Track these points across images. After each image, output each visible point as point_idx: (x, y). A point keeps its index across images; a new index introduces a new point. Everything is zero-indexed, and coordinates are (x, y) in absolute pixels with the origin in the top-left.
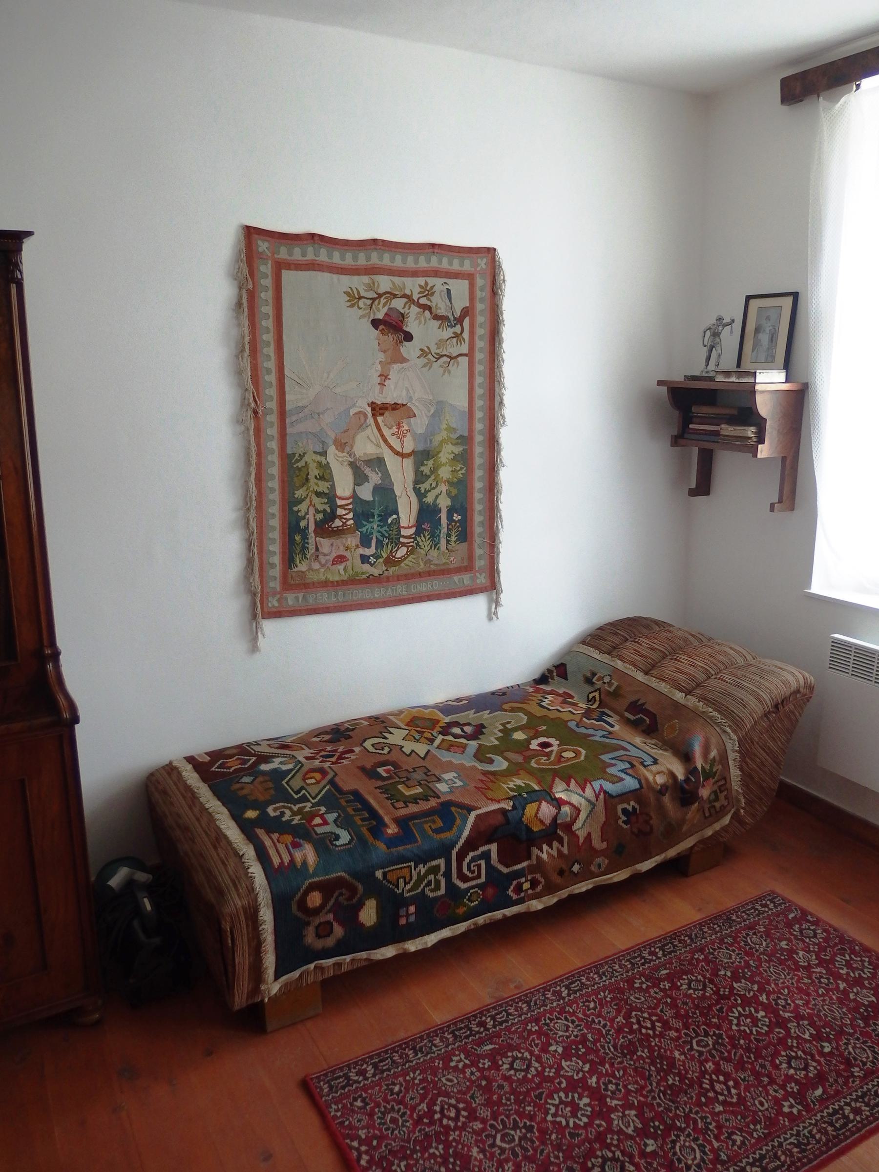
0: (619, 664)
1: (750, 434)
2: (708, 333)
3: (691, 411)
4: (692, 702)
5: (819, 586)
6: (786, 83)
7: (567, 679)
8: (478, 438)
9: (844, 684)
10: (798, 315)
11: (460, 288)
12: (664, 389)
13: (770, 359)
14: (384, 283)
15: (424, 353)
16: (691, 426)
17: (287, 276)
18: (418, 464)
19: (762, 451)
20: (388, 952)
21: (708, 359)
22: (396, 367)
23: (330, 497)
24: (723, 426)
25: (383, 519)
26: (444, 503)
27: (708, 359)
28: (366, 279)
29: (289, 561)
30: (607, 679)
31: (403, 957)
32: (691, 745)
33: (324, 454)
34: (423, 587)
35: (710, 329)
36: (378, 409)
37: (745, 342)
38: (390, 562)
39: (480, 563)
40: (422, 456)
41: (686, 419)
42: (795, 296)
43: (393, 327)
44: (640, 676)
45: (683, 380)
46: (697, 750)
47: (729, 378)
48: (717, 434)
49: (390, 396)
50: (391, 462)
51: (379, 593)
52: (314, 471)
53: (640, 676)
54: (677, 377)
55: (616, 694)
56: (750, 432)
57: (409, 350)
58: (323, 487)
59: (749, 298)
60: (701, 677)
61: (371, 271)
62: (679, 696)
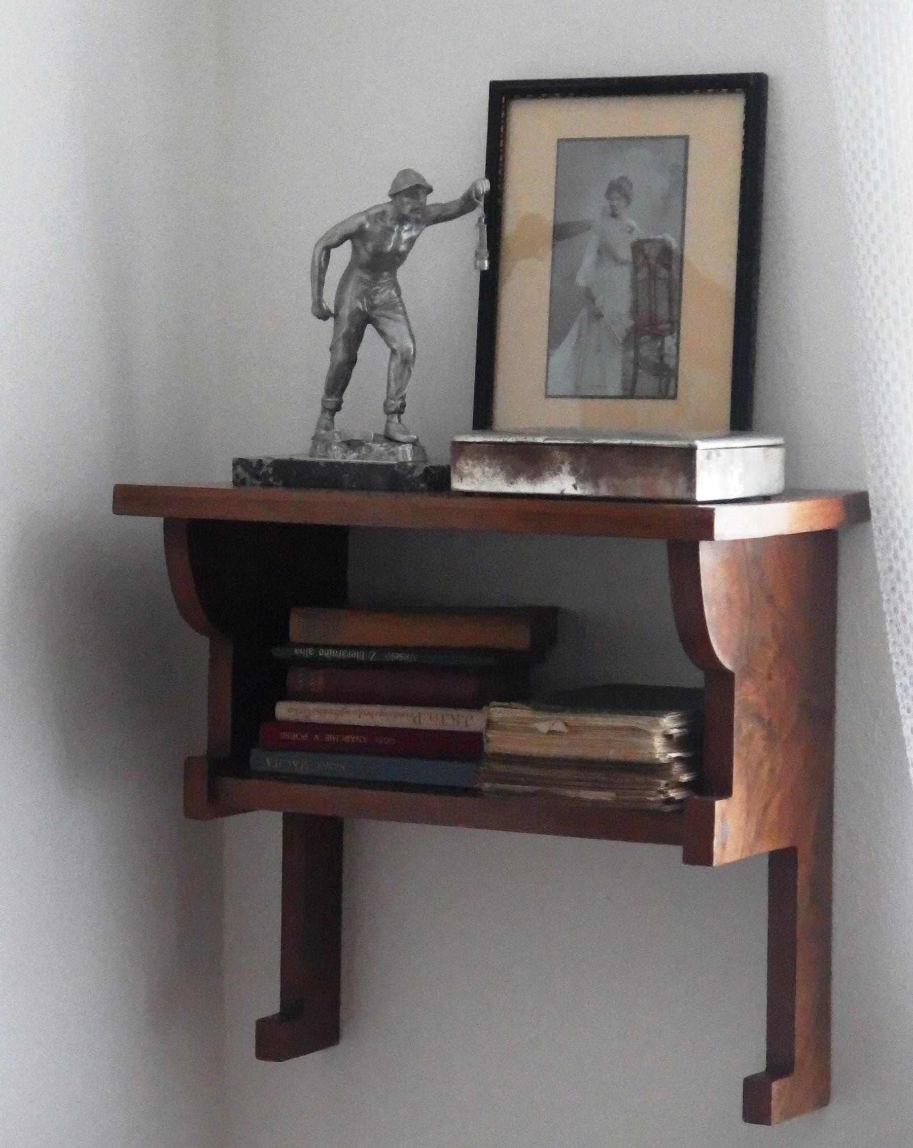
1: (660, 750)
2: (342, 256)
3: (282, 637)
7: (756, 1105)
10: (770, 136)
12: (151, 528)
13: (647, 382)
16: (284, 710)
19: (723, 846)
21: (338, 382)
24: (498, 712)
27: (338, 382)
35: (357, 236)
41: (255, 677)
42: (753, 90)
45: (230, 486)
47: (535, 475)
48: (469, 747)
56: (659, 738)
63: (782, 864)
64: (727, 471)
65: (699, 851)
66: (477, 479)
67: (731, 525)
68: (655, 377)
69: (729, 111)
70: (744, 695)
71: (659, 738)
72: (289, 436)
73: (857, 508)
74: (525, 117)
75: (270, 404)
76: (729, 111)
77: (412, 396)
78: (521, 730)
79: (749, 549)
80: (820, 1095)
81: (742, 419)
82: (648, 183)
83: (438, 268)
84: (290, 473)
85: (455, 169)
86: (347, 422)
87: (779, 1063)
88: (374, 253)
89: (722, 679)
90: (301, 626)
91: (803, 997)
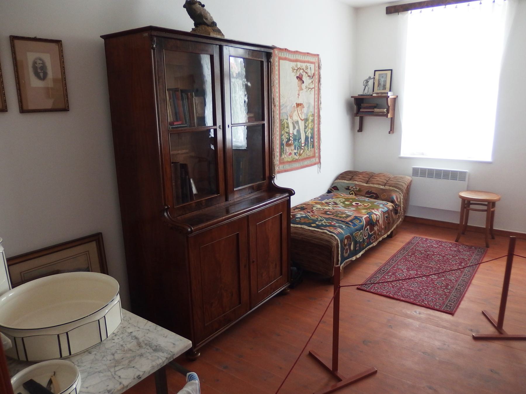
0: (357, 183)
4: (387, 187)
5: (402, 155)
6: (387, 8)
7: (389, 133)
8: (316, 115)
9: (418, 180)
11: (312, 66)
12: (353, 99)
14: (299, 64)
15: (306, 87)
17: (281, 61)
18: (305, 123)
20: (354, 258)
22: (301, 91)
23: (288, 133)
25: (298, 140)
26: (310, 136)
28: (295, 63)
29: (281, 155)
30: (354, 187)
31: (357, 259)
32: (393, 198)
33: (287, 119)
34: (306, 163)
36: (298, 105)
37: (260, 82)
38: (300, 155)
39: (317, 155)
40: (306, 120)
42: (391, 70)
43: (300, 78)
44: (365, 185)
46: (395, 199)
48: (373, 112)
49: (299, 102)
50: (300, 121)
51: (297, 165)
52: (286, 125)
53: (365, 185)
54: (356, 95)
55: (360, 190)
57: (304, 86)
58: (287, 131)
59: (375, 71)
60: (386, 182)
61: (296, 61)
62: (382, 187)
63: (392, 118)
64: (390, 94)
65: (387, 117)
66: (374, 95)
67: (390, 97)
68: (384, 88)
69: (390, 71)
70: (390, 108)
71: (385, 110)
72: (361, 93)
73: (397, 96)
74: (376, 72)
75: (359, 91)
76: (390, 71)
77: (368, 91)
78: (376, 110)
79: (252, 115)
80: (393, 133)
81: (390, 91)
82: (385, 76)
83: (371, 83)
84: (361, 95)
85: (372, 76)
86: (366, 91)
87: (391, 130)
88: (367, 81)
89: (389, 107)
90: (362, 105)
91: (56, 249)
